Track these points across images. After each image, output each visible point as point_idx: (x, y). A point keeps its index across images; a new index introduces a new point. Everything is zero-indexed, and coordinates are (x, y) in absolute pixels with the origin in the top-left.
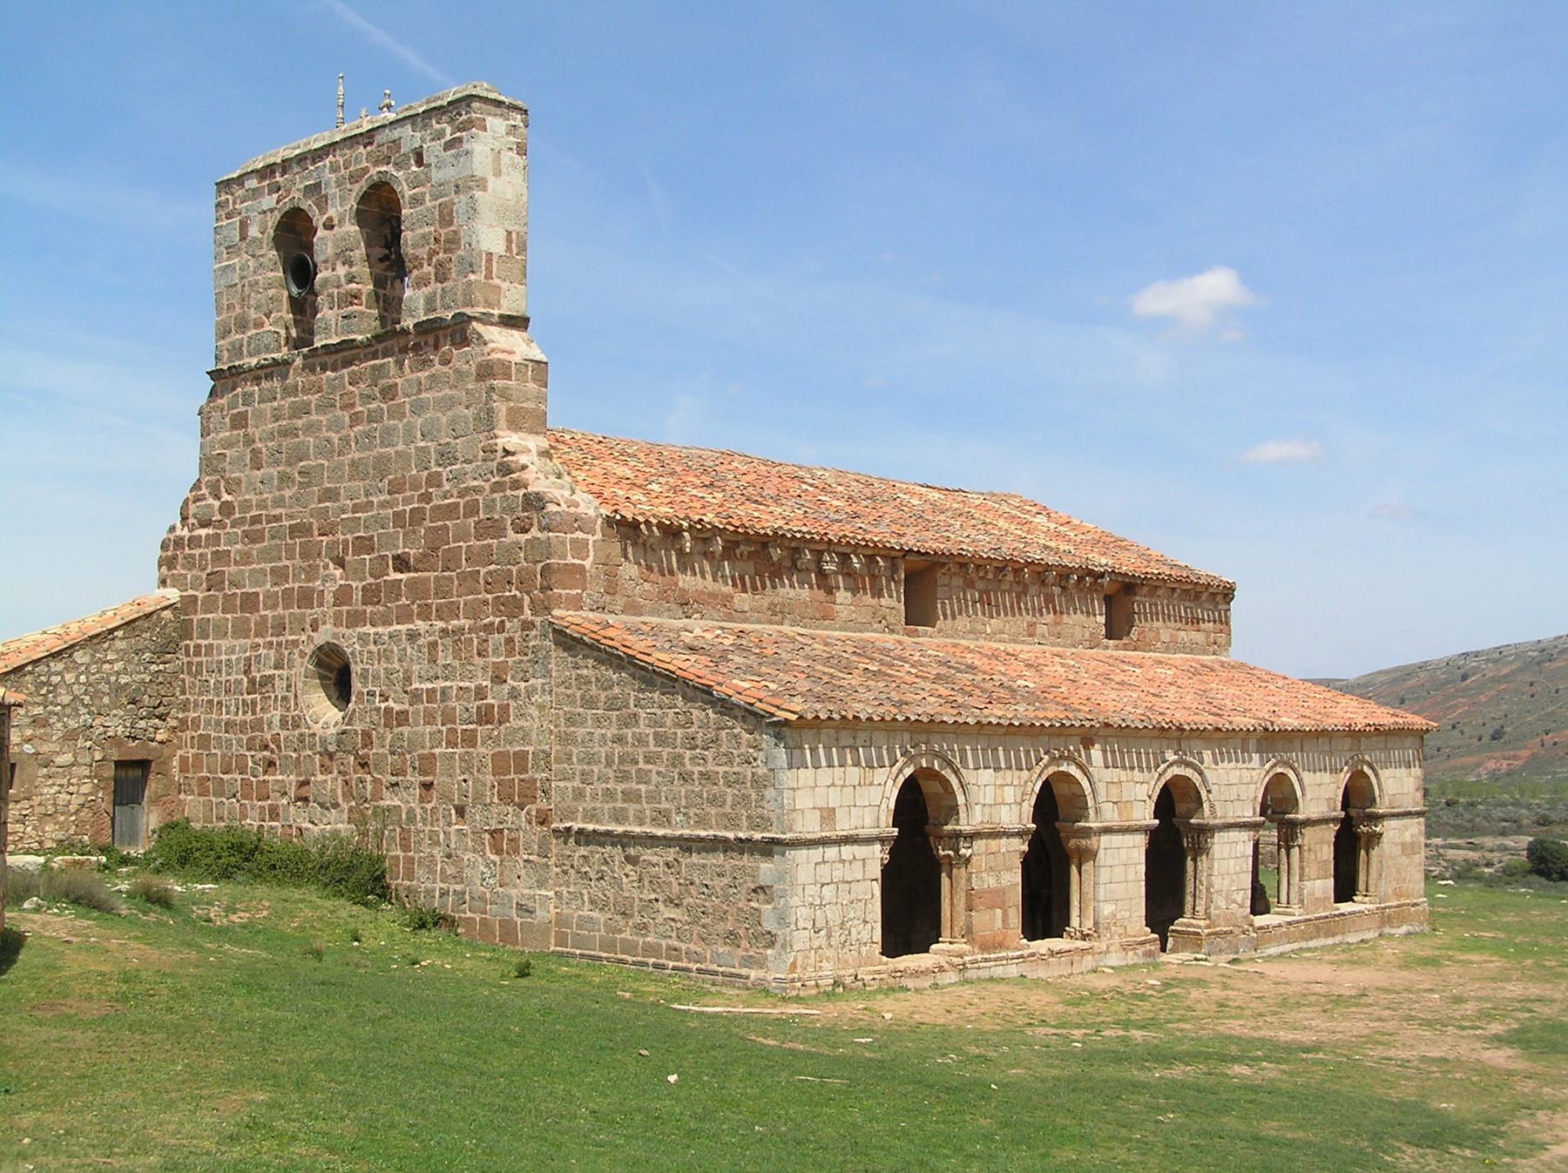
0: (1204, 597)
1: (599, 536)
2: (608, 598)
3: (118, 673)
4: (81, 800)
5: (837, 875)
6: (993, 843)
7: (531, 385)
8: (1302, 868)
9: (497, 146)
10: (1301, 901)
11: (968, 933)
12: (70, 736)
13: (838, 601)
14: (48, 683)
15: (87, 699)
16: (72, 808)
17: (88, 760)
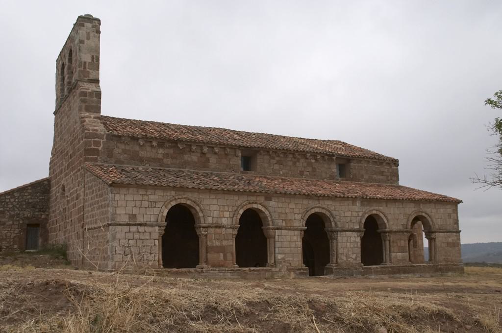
0: (384, 164)
1: (105, 140)
2: (108, 159)
3: (28, 199)
4: (15, 235)
5: (137, 236)
6: (218, 231)
7: (95, 98)
8: (390, 248)
9: (88, 31)
10: (390, 260)
11: (207, 262)
12: (12, 217)
13: (211, 162)
14: (5, 202)
15: (18, 206)
16: (12, 237)
17: (17, 223)
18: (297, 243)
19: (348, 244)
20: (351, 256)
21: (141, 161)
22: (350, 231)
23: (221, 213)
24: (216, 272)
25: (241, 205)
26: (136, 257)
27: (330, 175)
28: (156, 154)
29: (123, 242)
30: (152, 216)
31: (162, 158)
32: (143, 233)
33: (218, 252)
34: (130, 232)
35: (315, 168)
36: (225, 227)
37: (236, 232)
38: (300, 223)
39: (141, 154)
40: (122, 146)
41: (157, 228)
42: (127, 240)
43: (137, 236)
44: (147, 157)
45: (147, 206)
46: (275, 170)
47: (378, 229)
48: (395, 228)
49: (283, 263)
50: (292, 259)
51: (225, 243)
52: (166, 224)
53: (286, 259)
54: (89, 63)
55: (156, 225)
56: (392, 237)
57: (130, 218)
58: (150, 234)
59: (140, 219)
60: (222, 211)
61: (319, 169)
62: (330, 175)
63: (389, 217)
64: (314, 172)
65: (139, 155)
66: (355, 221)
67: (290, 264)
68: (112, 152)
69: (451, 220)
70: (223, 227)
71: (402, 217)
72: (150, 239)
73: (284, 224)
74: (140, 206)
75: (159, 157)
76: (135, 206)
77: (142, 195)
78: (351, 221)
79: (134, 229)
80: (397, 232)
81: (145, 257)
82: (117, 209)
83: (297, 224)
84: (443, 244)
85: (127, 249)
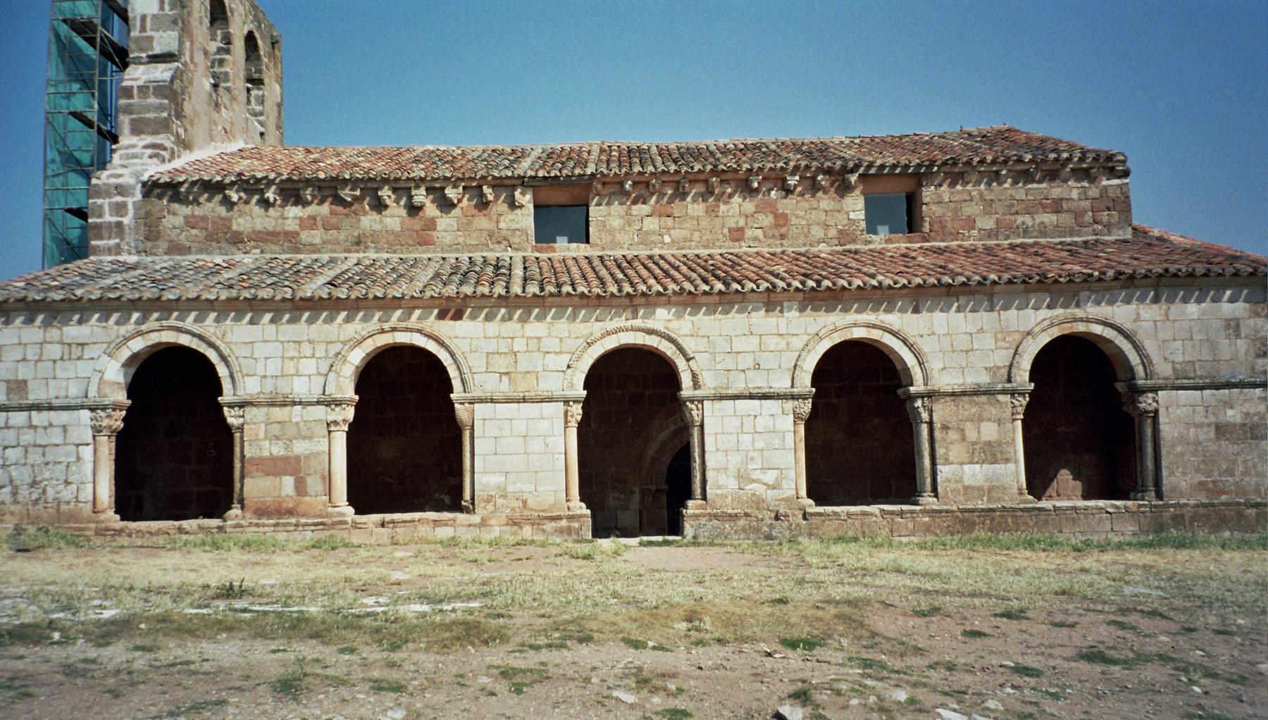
2: (149, 244)
5: (27, 437)
18: (550, 440)
19: (746, 439)
21: (237, 240)
24: (266, 529)
27: (840, 232)
28: (280, 221)
30: (72, 384)
31: (297, 228)
32: (45, 428)
33: (278, 474)
35: (785, 216)
36: (300, 403)
38: (111, 379)
40: (184, 210)
41: (86, 414)
44: (254, 231)
45: (58, 357)
46: (647, 233)
47: (221, 395)
48: (945, 381)
49: (500, 501)
50: (532, 487)
52: (357, 397)
53: (510, 489)
54: (154, 16)
55: (83, 407)
56: (942, 412)
57: (9, 391)
59: (36, 394)
60: (292, 358)
61: (797, 217)
62: (840, 232)
63: (925, 346)
64: (782, 226)
65: (229, 228)
66: (774, 365)
67: (525, 502)
68: (158, 226)
69: (1242, 345)
70: (294, 403)
71: (988, 342)
72: (66, 444)
74: (36, 358)
75: (287, 228)
76: (24, 360)
78: (757, 366)
79: (19, 418)
80: (964, 393)
83: (551, 384)
84: (1192, 430)
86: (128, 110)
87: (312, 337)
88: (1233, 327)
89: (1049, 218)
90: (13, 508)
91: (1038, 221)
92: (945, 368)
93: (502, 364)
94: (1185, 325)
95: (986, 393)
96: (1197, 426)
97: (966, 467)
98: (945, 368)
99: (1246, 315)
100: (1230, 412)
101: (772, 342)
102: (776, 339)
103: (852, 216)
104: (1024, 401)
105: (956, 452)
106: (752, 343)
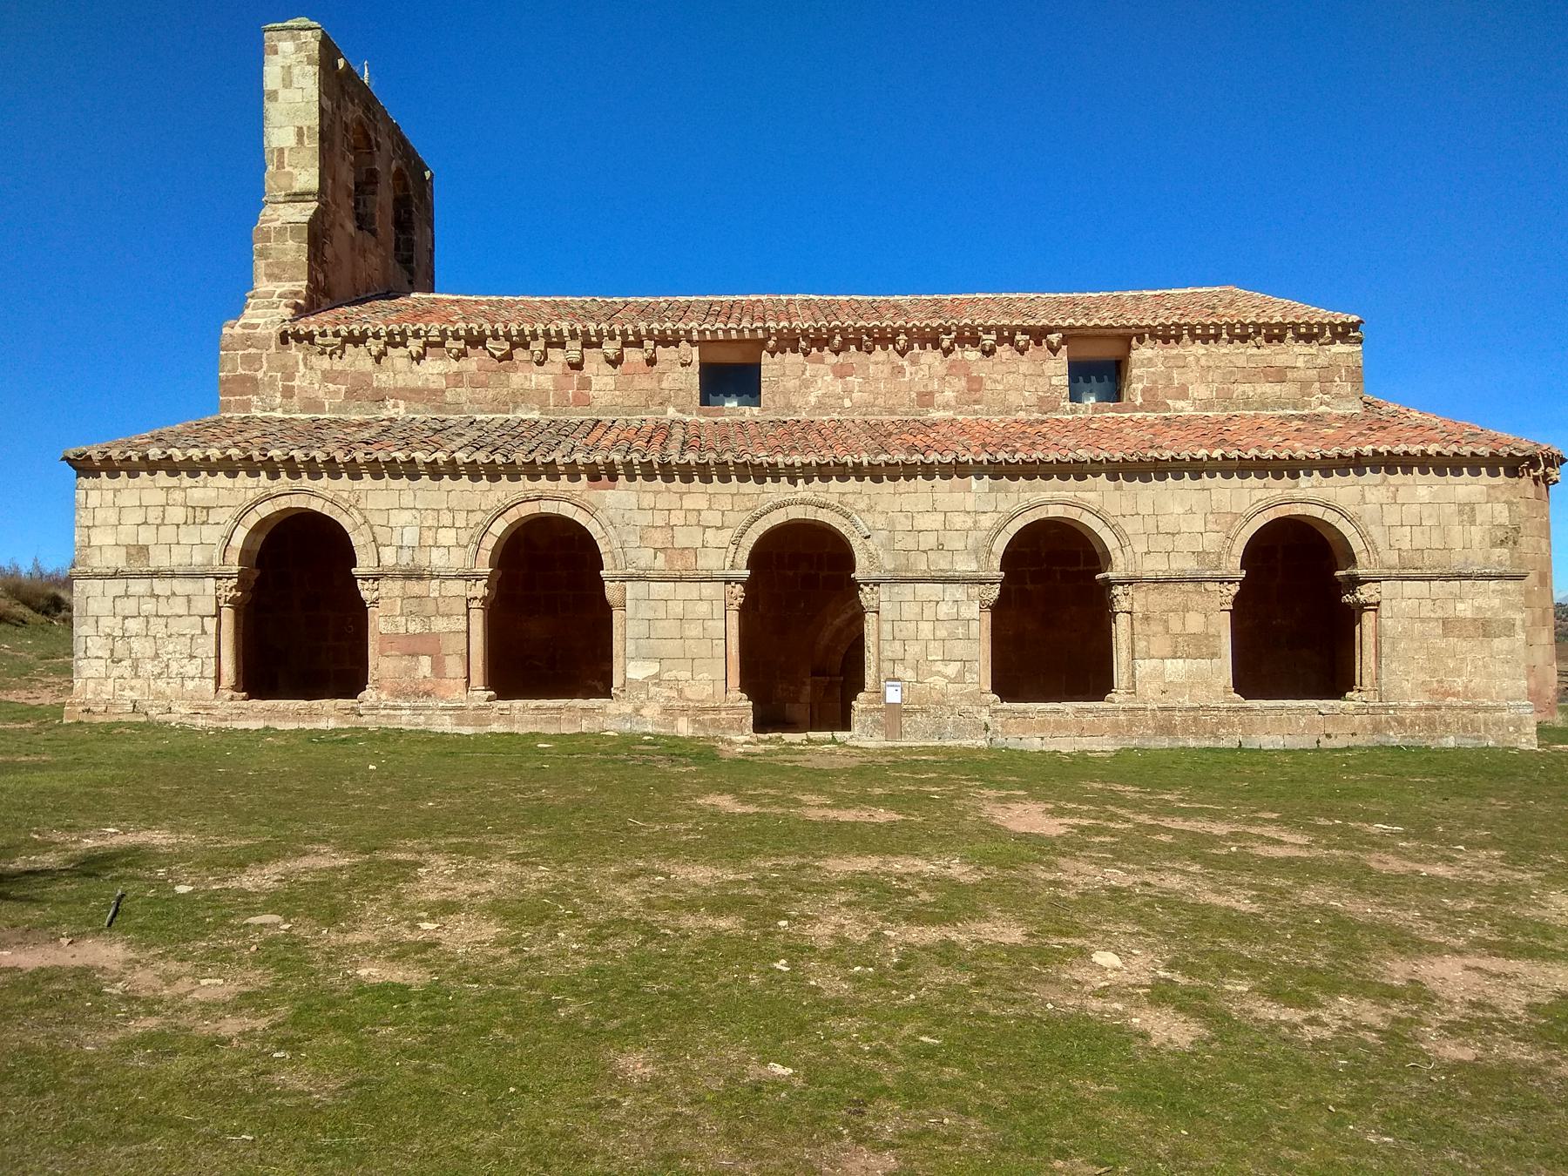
5: (149, 607)
6: (415, 587)
9: (288, 62)
20: (939, 666)
22: (934, 580)
23: (426, 533)
25: (492, 508)
26: (148, 667)
27: (1040, 399)
29: (107, 624)
32: (168, 598)
34: (127, 596)
37: (480, 590)
39: (379, 380)
42: (119, 619)
43: (149, 607)
49: (653, 690)
51: (439, 625)
53: (665, 676)
58: (189, 601)
59: (159, 559)
60: (429, 528)
61: (995, 381)
63: (1130, 527)
66: (961, 546)
67: (680, 691)
70: (432, 577)
73: (660, 562)
76: (145, 523)
77: (169, 488)
78: (940, 547)
79: (138, 587)
80: (1168, 581)
81: (174, 667)
82: (93, 532)
83: (712, 562)
84: (1417, 625)
85: (119, 644)
86: (263, 254)
87: (453, 504)
88: (1467, 511)
89: (1269, 389)
90: (133, 683)
91: (1259, 391)
92: (1148, 553)
93: (659, 538)
94: (1416, 508)
95: (1192, 580)
96: (1422, 620)
97: (1168, 662)
98: (1148, 553)
99: (1483, 499)
100: (1460, 606)
101: (959, 521)
102: (962, 517)
103: (1055, 381)
104: (1235, 589)
105: (1161, 644)
106: (935, 521)
